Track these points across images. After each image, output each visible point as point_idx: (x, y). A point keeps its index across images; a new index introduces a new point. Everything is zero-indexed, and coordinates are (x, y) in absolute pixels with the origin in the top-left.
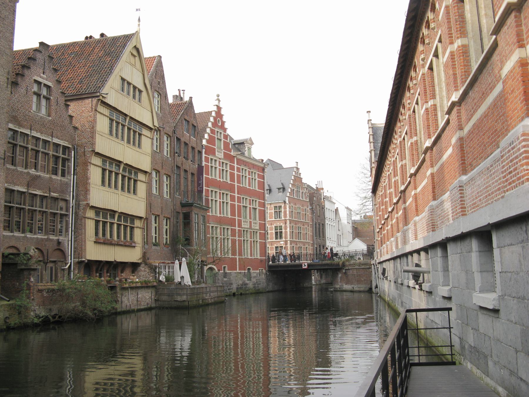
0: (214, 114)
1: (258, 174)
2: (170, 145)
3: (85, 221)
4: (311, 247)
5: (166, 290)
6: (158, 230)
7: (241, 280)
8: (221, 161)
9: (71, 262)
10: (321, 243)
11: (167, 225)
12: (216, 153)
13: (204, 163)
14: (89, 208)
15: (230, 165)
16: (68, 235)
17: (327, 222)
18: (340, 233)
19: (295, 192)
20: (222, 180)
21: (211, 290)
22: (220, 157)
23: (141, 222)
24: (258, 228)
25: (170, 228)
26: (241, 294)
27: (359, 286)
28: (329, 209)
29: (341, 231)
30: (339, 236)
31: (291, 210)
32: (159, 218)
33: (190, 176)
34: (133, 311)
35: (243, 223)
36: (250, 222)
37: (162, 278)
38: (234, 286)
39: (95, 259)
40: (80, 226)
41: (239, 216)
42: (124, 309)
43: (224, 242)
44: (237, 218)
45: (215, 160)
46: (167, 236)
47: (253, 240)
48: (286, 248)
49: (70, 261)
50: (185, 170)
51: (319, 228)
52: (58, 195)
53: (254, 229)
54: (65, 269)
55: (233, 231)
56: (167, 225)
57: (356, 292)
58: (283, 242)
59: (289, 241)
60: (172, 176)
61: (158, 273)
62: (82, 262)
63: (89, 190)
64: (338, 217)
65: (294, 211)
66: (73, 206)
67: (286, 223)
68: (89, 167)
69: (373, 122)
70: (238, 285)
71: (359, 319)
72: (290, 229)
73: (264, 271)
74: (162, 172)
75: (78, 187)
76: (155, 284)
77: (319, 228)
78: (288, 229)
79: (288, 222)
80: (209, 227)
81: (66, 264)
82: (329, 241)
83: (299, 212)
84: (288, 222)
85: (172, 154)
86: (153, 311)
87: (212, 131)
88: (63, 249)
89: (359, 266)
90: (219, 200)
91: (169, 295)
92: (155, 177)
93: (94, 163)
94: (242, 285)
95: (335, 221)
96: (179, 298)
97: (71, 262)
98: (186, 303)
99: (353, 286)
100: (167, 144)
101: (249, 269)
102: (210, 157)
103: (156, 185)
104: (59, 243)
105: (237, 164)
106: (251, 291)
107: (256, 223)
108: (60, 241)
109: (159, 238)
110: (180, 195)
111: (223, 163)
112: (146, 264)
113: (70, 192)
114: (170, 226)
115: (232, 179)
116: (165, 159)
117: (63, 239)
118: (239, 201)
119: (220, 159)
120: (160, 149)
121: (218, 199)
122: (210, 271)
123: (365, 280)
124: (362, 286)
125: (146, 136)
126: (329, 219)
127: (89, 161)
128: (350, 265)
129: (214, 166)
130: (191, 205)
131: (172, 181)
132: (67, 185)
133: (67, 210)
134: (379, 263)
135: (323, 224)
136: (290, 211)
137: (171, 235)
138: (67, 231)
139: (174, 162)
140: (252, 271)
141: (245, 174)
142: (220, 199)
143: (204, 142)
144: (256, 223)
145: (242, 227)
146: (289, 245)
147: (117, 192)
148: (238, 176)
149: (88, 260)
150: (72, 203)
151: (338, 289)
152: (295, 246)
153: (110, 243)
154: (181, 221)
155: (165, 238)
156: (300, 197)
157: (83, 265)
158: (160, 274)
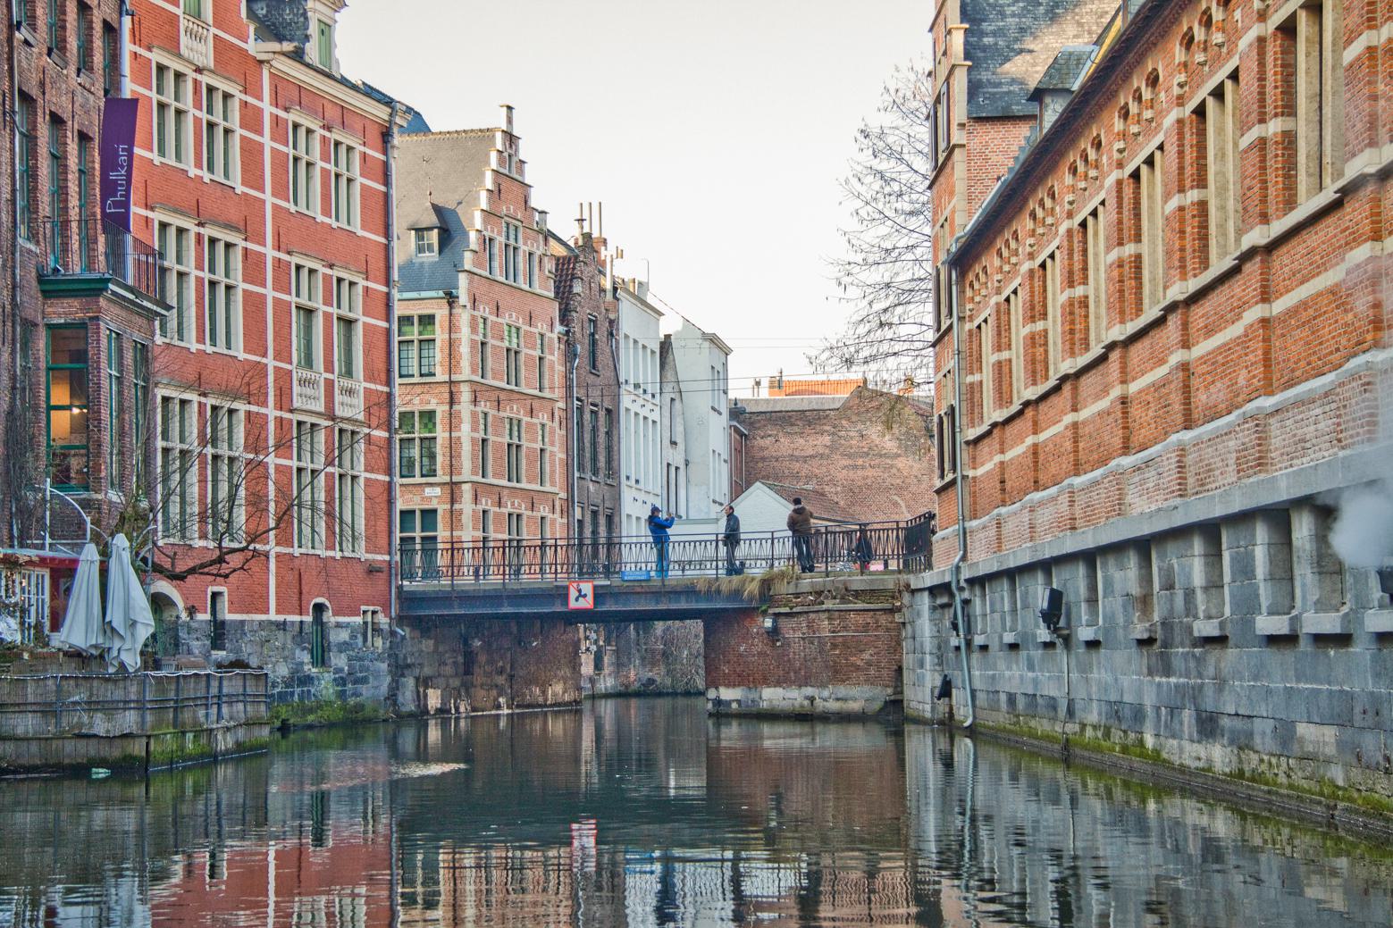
4: (561, 521)
7: (285, 659)
8: (205, 79)
10: (599, 501)
12: (184, 40)
13: (129, 88)
17: (626, 401)
18: (677, 458)
19: (496, 250)
20: (207, 177)
27: (842, 690)
28: (635, 342)
29: (681, 446)
30: (673, 470)
31: (480, 338)
35: (296, 389)
36: (329, 385)
41: (283, 353)
43: (215, 472)
44: (270, 362)
50: (53, 115)
51: (594, 430)
53: (343, 419)
57: (826, 718)
58: (438, 491)
59: (466, 487)
64: (669, 375)
65: (491, 341)
67: (452, 401)
72: (474, 429)
77: (594, 430)
79: (465, 394)
82: (634, 493)
83: (514, 346)
84: (465, 394)
89: (843, 600)
90: (194, 273)
91: (48, 710)
95: (657, 400)
98: (137, 748)
99: (809, 691)
101: (319, 608)
102: (156, 56)
106: (325, 714)
107: (350, 392)
115: (253, 175)
118: (281, 285)
119: (199, 70)
121: (190, 266)
123: (869, 664)
124: (854, 691)
126: (637, 386)
128: (797, 595)
129: (174, 104)
135: (609, 411)
140: (329, 617)
142: (200, 267)
144: (350, 392)
145: (296, 405)
146: (466, 505)
151: (734, 705)
152: (493, 509)
156: (521, 278)
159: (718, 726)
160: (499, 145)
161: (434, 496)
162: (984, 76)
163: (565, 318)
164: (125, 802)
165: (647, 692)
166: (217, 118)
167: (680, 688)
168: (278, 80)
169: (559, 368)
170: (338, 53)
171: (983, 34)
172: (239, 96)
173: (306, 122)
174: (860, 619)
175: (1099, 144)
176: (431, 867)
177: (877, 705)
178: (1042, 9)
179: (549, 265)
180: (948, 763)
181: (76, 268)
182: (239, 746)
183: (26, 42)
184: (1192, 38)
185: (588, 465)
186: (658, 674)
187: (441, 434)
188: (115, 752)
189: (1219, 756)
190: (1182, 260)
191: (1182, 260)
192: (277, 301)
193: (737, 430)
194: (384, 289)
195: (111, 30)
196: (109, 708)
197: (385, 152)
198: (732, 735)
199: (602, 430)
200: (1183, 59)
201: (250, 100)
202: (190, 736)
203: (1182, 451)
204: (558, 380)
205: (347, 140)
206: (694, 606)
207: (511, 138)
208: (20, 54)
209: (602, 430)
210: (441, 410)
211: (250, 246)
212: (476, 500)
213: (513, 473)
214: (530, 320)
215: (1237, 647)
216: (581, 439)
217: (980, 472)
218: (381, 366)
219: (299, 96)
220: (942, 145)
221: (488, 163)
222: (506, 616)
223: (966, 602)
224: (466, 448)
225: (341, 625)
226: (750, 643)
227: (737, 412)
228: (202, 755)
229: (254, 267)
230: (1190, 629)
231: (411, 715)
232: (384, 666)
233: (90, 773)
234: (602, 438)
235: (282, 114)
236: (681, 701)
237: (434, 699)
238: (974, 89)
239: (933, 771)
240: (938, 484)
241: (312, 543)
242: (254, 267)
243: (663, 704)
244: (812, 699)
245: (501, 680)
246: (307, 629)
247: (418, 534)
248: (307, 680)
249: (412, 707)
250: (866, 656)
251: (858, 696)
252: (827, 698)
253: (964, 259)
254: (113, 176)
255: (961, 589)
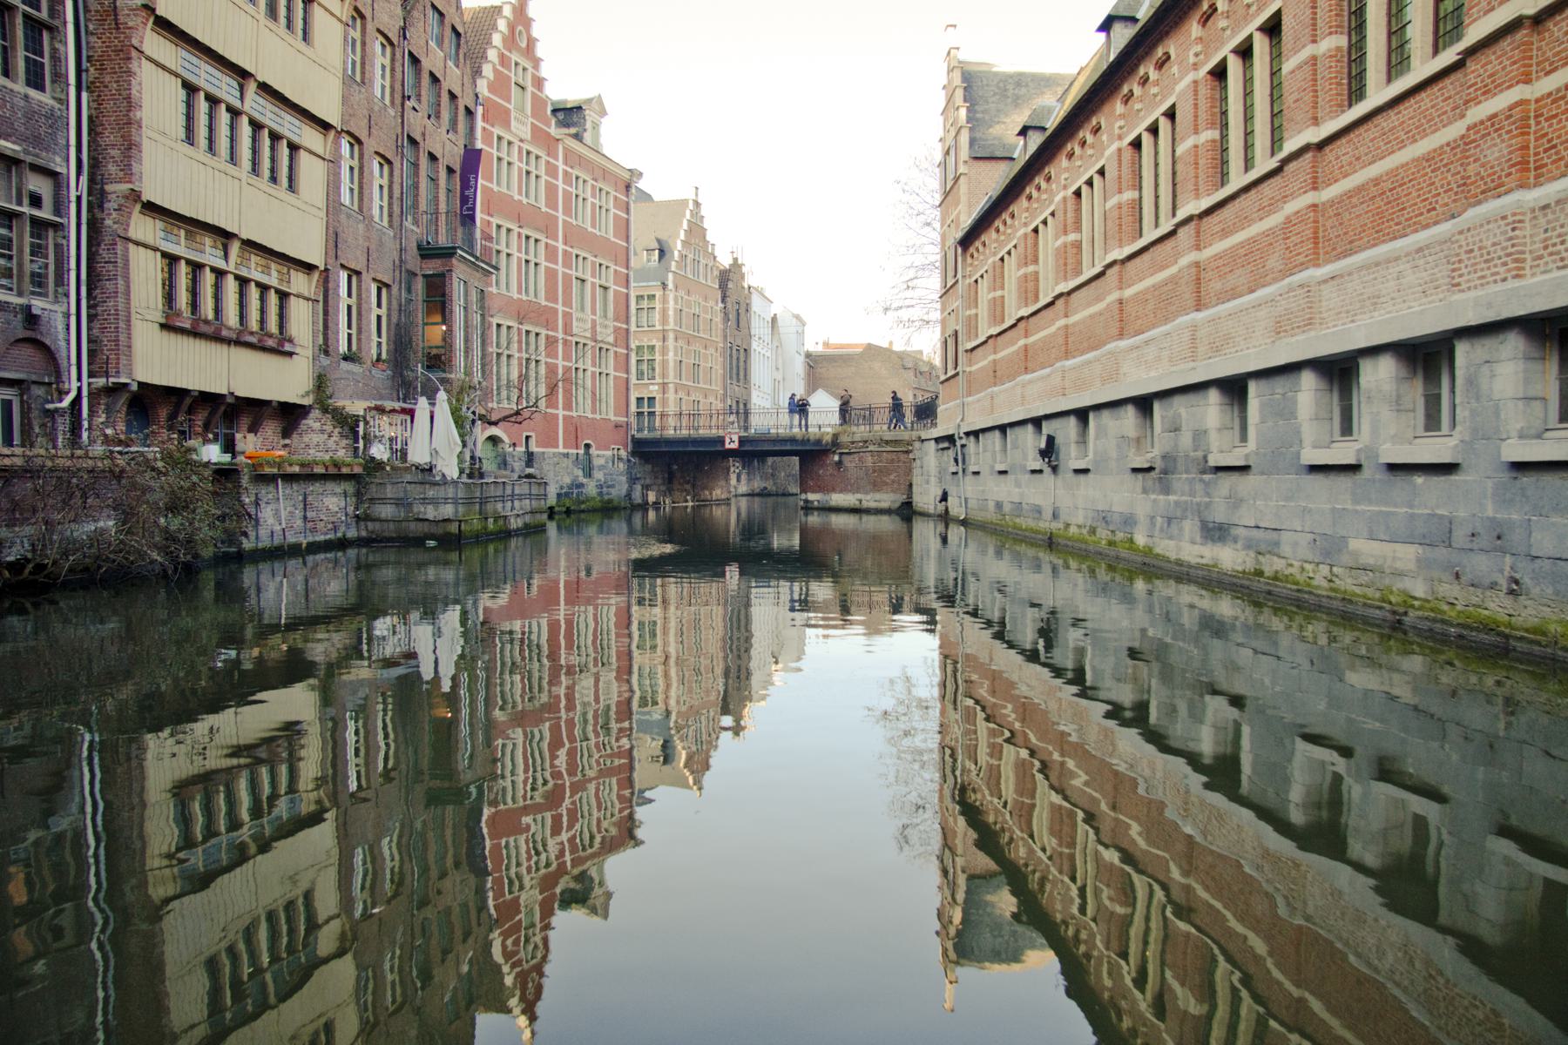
0: (507, 11)
1: (616, 198)
2: (393, 70)
3: (127, 250)
5: (389, 487)
6: (356, 315)
9: (80, 389)
11: (379, 306)
12: (513, 123)
14: (138, 207)
15: (548, 337)
16: (67, 295)
17: (754, 345)
18: (779, 377)
20: (525, 201)
21: (516, 492)
22: (523, 136)
23: (310, 281)
24: (611, 339)
25: (389, 316)
26: (568, 512)
27: (878, 496)
32: (359, 282)
33: (443, 174)
34: (294, 551)
35: (575, 323)
36: (594, 322)
37: (379, 452)
38: (552, 491)
39: (164, 383)
40: (111, 267)
41: (567, 303)
42: (265, 542)
44: (560, 308)
45: (510, 143)
46: (379, 335)
47: (598, 370)
48: (664, 402)
49: (75, 385)
50: (430, 153)
52: (17, 148)
54: (56, 410)
55: (551, 342)
56: (379, 306)
57: (868, 511)
58: (656, 387)
60: (397, 165)
61: (364, 438)
62: (116, 390)
63: (138, 146)
65: (685, 309)
66: (79, 198)
67: (664, 340)
68: (134, 66)
69: (963, 56)
70: (562, 488)
71: (514, 562)
72: (676, 355)
73: (623, 453)
74: (370, 145)
75: (97, 134)
76: (358, 470)
78: (671, 354)
79: (671, 336)
80: (490, 325)
81: (62, 393)
84: (671, 336)
85: (398, 101)
86: (352, 553)
87: (503, 60)
88: (48, 342)
90: (516, 254)
91: (398, 502)
92: (348, 156)
93: (155, 57)
94: (571, 487)
96: (430, 513)
97: (80, 389)
98: (454, 528)
99: (859, 496)
100: (383, 67)
101: (587, 446)
102: (497, 131)
103: (352, 182)
104: (31, 319)
105: (566, 163)
107: (606, 327)
108: (35, 311)
109: (359, 340)
110: (416, 222)
111: (528, 153)
112: (325, 410)
113: (68, 146)
114: (389, 309)
115: (552, 202)
116: (376, 108)
117: (48, 306)
118: (567, 264)
119: (521, 141)
120: (363, 73)
122: (489, 446)
123: (893, 482)
125: (326, 9)
127: (135, 42)
128: (853, 443)
130: (448, 253)
131: (397, 179)
132: (55, 121)
133: (59, 208)
134: (968, 434)
136: (675, 309)
137: (392, 333)
138: (61, 279)
139: (403, 122)
140: (593, 451)
141: (507, 246)
142: (519, 250)
143: (483, 87)
144: (606, 327)
146: (671, 395)
147: (236, 174)
148: (567, 194)
149: (140, 384)
150: (77, 187)
153: (212, 334)
154: (420, 298)
155: (376, 344)
157: (122, 401)
158: (368, 440)
159: (806, 515)
160: (691, 207)
161: (654, 390)
162: (978, 135)
163: (723, 301)
164: (447, 563)
165: (763, 494)
166: (532, 169)
167: (780, 491)
168: (567, 152)
169: (721, 326)
170: (603, 140)
171: (976, 112)
172: (544, 157)
173: (583, 176)
174: (889, 456)
175: (1050, 178)
176: (653, 586)
177: (897, 505)
178: (1009, 100)
179: (716, 273)
180: (944, 540)
181: (443, 240)
182: (526, 526)
183: (414, 109)
184: (1148, 79)
185: (734, 376)
186: (769, 485)
187: (658, 357)
188: (439, 530)
189: (1230, 558)
190: (1196, 184)
191: (1196, 184)
192: (564, 274)
193: (249, 934)
194: (626, 271)
195: (469, 112)
196: (435, 502)
197: (627, 196)
198: (814, 519)
199: (742, 359)
200: (1226, 9)
201: (551, 160)
202: (491, 520)
203: (1194, 328)
204: (720, 333)
205: (606, 188)
206: (795, 448)
207: (697, 204)
208: (409, 114)
209: (742, 359)
210: (658, 344)
211: (549, 241)
212: (676, 392)
213: (695, 379)
214: (706, 299)
215: (1262, 473)
216: (731, 364)
217: (974, 368)
218: (623, 313)
219: (581, 161)
220: (951, 176)
221: (684, 216)
222: (691, 452)
223: (963, 446)
224: (671, 364)
225: (601, 456)
226: (826, 472)
227: (808, 355)
228: (500, 532)
229: (551, 254)
230: (1025, 467)
231: (639, 505)
232: (624, 479)
233: (424, 544)
234: (742, 364)
235: (569, 169)
236: (781, 500)
237: (652, 497)
238: (972, 142)
239: (934, 543)
240: (943, 378)
241: (583, 409)
242: (551, 254)
243: (770, 500)
244: (860, 501)
245: (688, 487)
246: (581, 457)
247: (646, 409)
248: (581, 485)
249: (640, 501)
250: (892, 477)
251: (887, 499)
252: (870, 500)
253: (966, 242)
254: (467, 193)
255: (960, 438)
